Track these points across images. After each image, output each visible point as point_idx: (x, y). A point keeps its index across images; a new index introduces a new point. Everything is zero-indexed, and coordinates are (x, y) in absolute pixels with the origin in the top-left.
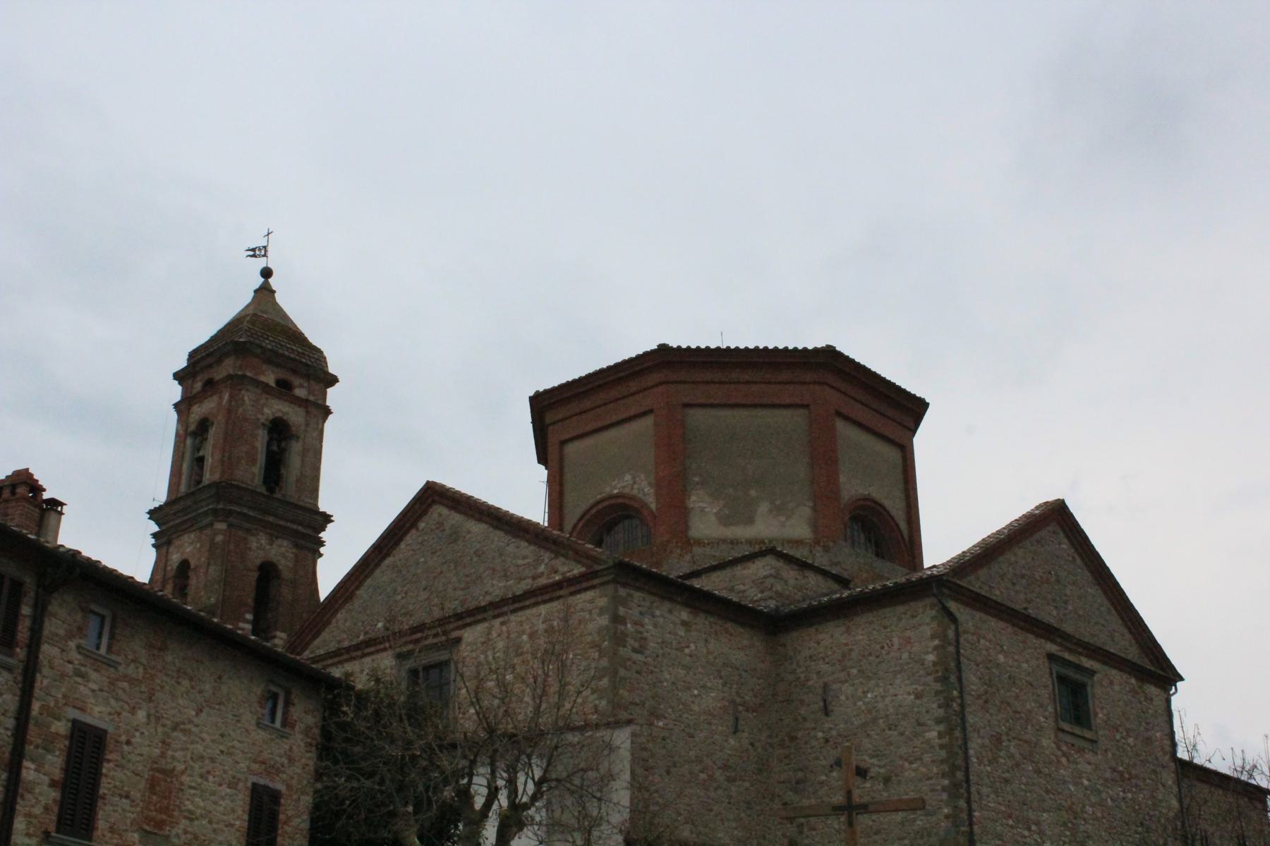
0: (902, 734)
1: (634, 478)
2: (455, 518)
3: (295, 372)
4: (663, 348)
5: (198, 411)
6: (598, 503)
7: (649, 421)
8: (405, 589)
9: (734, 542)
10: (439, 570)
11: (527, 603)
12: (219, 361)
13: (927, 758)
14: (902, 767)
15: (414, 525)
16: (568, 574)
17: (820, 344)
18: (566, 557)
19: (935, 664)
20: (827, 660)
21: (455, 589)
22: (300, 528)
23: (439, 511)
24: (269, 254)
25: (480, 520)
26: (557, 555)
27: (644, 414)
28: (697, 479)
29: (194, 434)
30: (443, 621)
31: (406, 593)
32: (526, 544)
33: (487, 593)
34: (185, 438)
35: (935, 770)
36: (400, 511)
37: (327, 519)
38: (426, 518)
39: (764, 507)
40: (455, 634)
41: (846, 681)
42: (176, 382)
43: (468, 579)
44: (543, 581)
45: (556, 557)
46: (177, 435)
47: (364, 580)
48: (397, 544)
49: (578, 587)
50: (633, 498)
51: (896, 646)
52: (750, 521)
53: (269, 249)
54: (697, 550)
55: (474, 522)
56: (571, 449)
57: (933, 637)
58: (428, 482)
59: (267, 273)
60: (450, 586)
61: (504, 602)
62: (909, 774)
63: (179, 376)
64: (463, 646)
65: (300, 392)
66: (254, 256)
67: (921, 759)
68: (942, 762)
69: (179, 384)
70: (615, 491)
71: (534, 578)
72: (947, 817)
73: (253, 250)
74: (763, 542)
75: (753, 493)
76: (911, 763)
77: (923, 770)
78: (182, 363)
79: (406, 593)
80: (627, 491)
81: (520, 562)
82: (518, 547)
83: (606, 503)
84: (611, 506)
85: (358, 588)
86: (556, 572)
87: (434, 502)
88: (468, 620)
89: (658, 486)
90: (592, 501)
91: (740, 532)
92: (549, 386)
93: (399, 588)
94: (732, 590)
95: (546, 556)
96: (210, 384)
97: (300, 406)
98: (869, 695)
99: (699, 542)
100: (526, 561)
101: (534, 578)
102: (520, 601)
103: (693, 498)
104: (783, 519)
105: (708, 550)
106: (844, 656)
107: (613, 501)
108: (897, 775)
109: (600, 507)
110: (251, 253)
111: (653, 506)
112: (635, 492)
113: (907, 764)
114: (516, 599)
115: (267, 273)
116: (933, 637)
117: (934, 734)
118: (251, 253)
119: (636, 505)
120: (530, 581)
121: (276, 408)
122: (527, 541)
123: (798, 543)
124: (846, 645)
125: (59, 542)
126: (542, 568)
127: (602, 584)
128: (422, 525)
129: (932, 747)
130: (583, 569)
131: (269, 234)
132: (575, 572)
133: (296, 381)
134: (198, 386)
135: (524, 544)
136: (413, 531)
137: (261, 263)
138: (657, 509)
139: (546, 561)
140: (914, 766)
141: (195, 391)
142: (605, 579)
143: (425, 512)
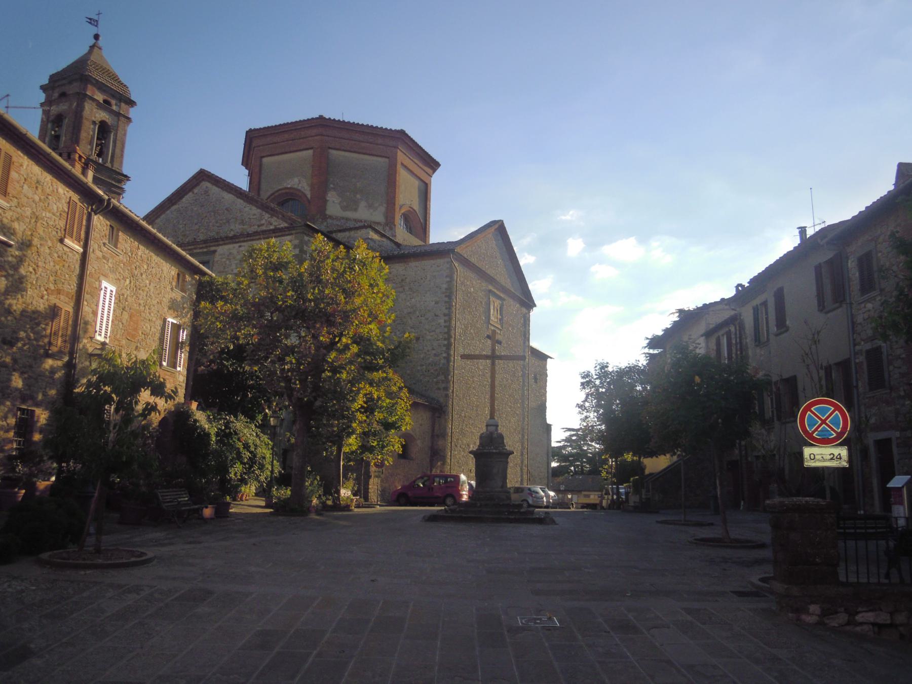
0: (427, 319)
1: (299, 181)
2: (215, 190)
3: (113, 96)
4: (321, 118)
5: (55, 110)
6: (280, 190)
7: (310, 152)
8: (184, 223)
9: (347, 219)
10: (205, 215)
11: (255, 238)
12: (70, 83)
13: (438, 331)
14: (426, 334)
15: (191, 190)
16: (278, 227)
17: (398, 128)
18: (278, 218)
19: (446, 289)
20: (394, 281)
21: (213, 226)
22: (114, 183)
23: (205, 184)
24: (99, 26)
25: (229, 192)
26: (272, 216)
27: (386, 157)
28: (332, 186)
29: (53, 122)
30: (205, 242)
31: (185, 225)
32: (255, 208)
33: (232, 230)
34: (47, 124)
35: (441, 337)
36: (185, 181)
37: (127, 178)
38: (198, 188)
39: (363, 204)
40: (213, 249)
41: (402, 292)
42: (41, 91)
43: (221, 222)
44: (264, 228)
45: (271, 217)
46: (42, 121)
47: (161, 215)
48: (181, 198)
49: (284, 233)
50: (299, 190)
51: (428, 279)
52: (356, 210)
53: (99, 22)
54: (329, 221)
55: (226, 193)
56: (265, 160)
57: (447, 277)
58: (201, 169)
59: (96, 37)
60: (211, 224)
61: (242, 235)
62: (429, 337)
63: (44, 88)
64: (217, 253)
65: (114, 108)
66: (90, 23)
67: (435, 331)
68: (445, 333)
69: (43, 92)
70: (289, 186)
71: (259, 226)
72: (444, 358)
73: (90, 19)
74: (361, 221)
75: (358, 196)
76: (430, 332)
77: (436, 336)
78: (46, 81)
79: (185, 225)
80: (296, 186)
81: (252, 217)
82: (250, 209)
83: (283, 191)
84: (286, 193)
85: (156, 218)
86: (271, 224)
87: (203, 180)
88: (221, 243)
89: (312, 186)
90: (276, 189)
91: (349, 214)
92: (257, 127)
93: (181, 222)
94: (349, 242)
95: (267, 216)
96: (63, 95)
97: (115, 116)
98: (413, 300)
99: (330, 217)
100: (255, 217)
101: (259, 226)
102: (251, 236)
103: (329, 195)
104: (372, 211)
105: (335, 222)
106: (402, 280)
107: (287, 191)
108: (422, 337)
109: (280, 192)
110: (89, 21)
111: (309, 196)
112: (299, 188)
113: (428, 333)
114: (248, 235)
115: (96, 37)
116: (447, 277)
117: (443, 321)
118: (89, 21)
119: (300, 194)
120: (256, 227)
121: (102, 115)
122: (256, 206)
123: (378, 223)
124: (404, 275)
125: (584, 245)
126: (263, 222)
127: (296, 233)
128: (196, 191)
129: (441, 326)
130: (286, 225)
131: (99, 14)
132: (282, 226)
133: (113, 102)
134: (56, 95)
135: (254, 208)
136: (190, 194)
137: (94, 30)
138: (311, 198)
139: (266, 218)
140: (431, 334)
141: (53, 98)
142: (298, 231)
143: (197, 185)
